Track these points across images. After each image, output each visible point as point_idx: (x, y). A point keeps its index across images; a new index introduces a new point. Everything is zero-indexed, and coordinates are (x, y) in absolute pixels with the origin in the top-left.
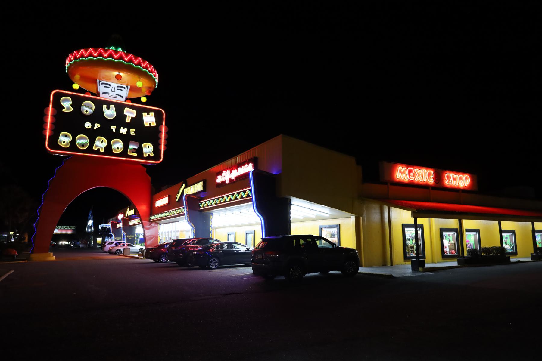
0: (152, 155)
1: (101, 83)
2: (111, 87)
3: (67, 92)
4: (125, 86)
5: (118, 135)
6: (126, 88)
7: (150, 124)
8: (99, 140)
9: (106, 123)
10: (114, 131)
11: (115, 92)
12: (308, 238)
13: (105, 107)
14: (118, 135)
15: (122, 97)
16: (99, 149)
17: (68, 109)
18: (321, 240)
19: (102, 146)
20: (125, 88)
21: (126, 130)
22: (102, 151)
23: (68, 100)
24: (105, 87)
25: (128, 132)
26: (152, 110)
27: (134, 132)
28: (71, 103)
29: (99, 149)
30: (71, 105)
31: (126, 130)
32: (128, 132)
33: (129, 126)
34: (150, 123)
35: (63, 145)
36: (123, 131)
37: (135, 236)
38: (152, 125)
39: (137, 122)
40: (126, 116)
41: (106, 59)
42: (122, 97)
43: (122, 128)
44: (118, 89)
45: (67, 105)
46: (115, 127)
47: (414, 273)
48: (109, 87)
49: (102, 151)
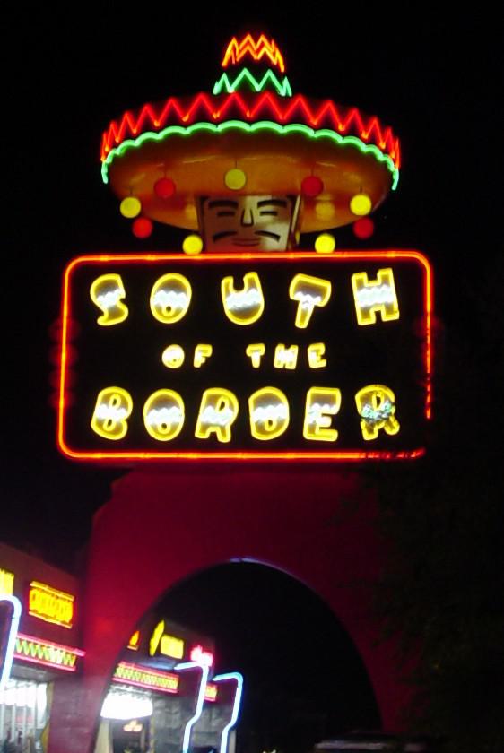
0: (394, 429)
3: (104, 258)
5: (269, 375)
7: (378, 314)
8: (212, 400)
9: (229, 339)
10: (256, 363)
12: (319, 742)
14: (269, 375)
16: (213, 435)
17: (114, 313)
19: (222, 423)
21: (294, 349)
22: (225, 438)
23: (109, 287)
25: (303, 357)
26: (385, 264)
28: (120, 292)
29: (213, 435)
30: (123, 301)
31: (294, 349)
32: (303, 357)
33: (302, 340)
34: (377, 309)
35: (104, 432)
36: (286, 357)
38: (385, 318)
39: (338, 313)
40: (295, 304)
41: (221, 128)
45: (110, 301)
46: (206, 351)
49: (225, 438)
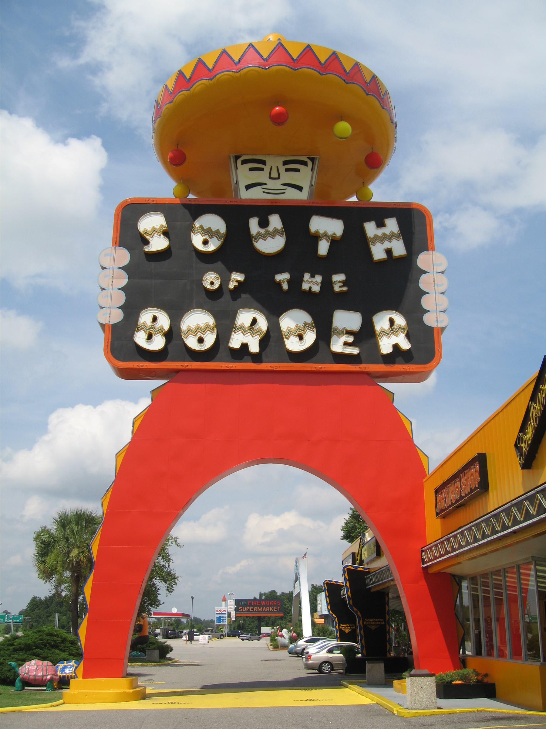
1: (239, 162)
2: (267, 169)
4: (305, 159)
6: (310, 163)
11: (279, 178)
13: (254, 225)
15: (300, 188)
18: (363, 560)
20: (305, 164)
24: (264, 192)
25: (327, 284)
27: (345, 283)
32: (327, 284)
37: (385, 621)
42: (300, 188)
43: (316, 289)
44: (287, 170)
47: (529, 573)
48: (262, 169)
